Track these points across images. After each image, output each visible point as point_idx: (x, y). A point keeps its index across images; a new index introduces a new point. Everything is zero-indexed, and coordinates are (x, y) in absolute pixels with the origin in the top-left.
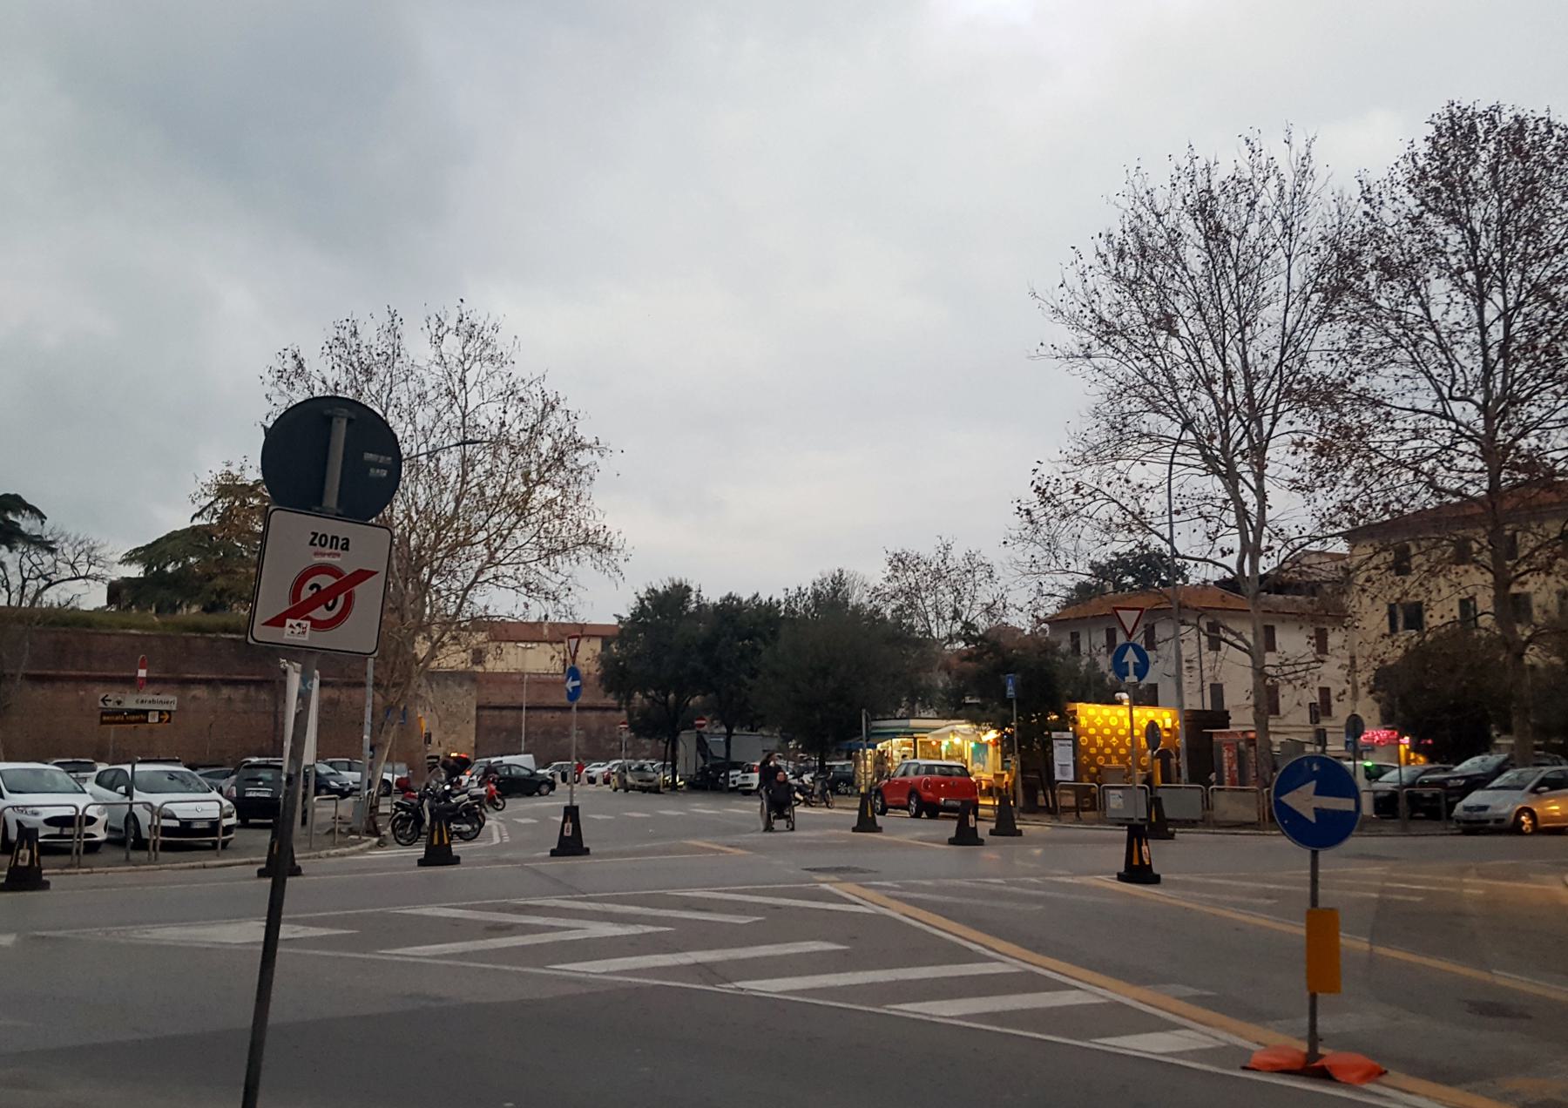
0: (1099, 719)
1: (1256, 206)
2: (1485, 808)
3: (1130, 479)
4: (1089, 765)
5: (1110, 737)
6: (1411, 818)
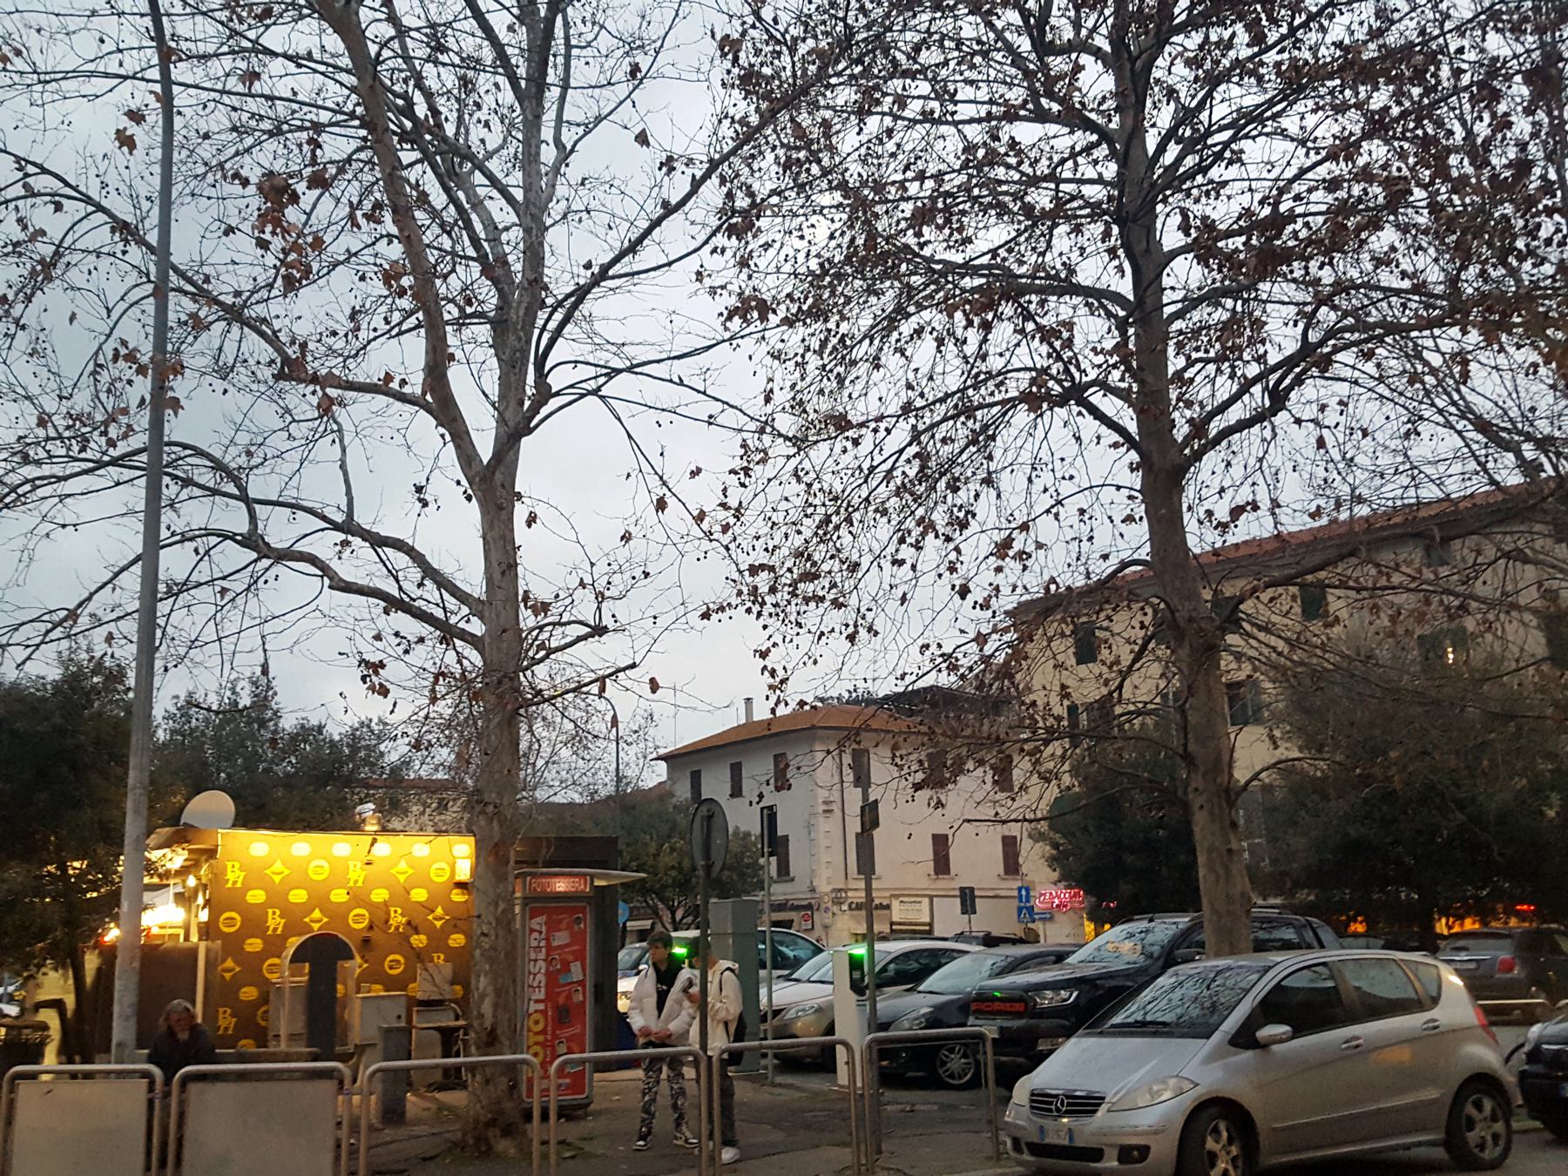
0: (278, 867)
1: (970, 247)
2: (1086, 1104)
3: (584, 262)
4: (237, 983)
5: (307, 908)
6: (384, 830)
